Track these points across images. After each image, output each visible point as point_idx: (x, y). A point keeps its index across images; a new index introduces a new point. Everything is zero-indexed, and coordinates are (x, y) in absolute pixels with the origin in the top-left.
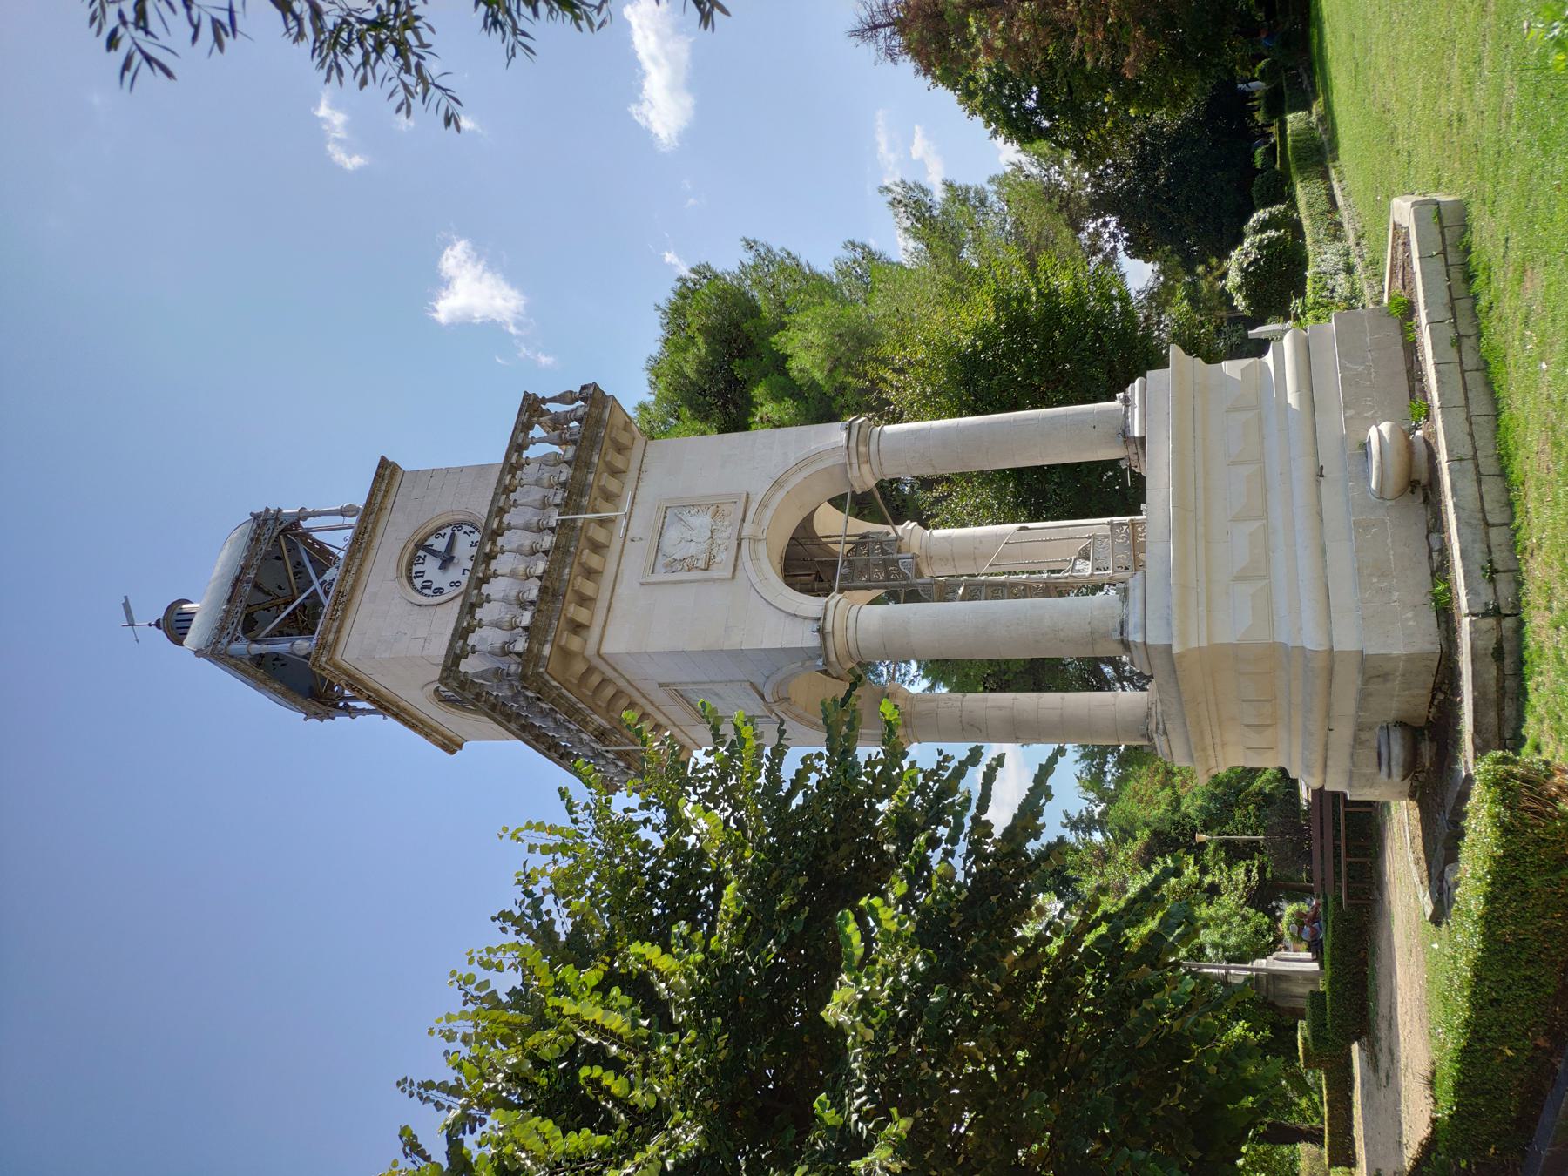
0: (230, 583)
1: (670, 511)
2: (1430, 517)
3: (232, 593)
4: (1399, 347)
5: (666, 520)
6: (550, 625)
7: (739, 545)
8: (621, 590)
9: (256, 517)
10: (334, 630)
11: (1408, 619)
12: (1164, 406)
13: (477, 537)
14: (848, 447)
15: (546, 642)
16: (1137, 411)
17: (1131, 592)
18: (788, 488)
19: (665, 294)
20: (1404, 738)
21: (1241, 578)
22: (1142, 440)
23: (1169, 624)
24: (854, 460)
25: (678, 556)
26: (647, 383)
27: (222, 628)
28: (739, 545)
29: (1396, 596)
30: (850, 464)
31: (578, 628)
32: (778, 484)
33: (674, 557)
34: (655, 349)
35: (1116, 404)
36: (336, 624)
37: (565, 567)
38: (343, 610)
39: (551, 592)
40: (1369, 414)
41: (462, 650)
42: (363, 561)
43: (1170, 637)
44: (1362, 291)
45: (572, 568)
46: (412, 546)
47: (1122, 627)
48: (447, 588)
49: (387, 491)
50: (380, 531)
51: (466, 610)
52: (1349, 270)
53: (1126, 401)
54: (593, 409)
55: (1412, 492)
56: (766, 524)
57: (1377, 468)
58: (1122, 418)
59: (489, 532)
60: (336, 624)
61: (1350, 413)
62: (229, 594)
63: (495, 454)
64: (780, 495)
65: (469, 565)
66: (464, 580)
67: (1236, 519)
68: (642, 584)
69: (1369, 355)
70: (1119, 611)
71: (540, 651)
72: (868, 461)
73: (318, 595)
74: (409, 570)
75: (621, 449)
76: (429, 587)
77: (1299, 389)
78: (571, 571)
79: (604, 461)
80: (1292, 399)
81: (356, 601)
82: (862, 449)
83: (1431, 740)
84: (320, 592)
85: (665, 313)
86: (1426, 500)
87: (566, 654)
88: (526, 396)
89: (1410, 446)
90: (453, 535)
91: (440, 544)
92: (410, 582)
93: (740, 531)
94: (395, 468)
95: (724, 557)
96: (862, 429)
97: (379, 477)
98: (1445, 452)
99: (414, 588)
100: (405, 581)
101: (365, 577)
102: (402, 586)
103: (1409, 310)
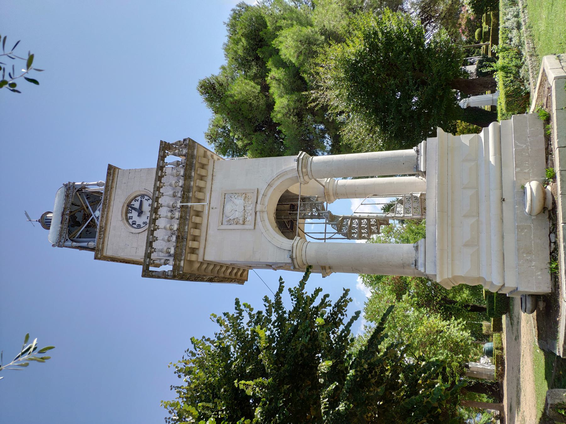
0: (60, 215)
1: (226, 196)
2: (551, 225)
3: (62, 219)
4: (543, 136)
5: (226, 200)
6: (182, 252)
7: (256, 213)
8: (210, 232)
9: (66, 185)
10: (101, 243)
11: (538, 275)
12: (434, 157)
13: (150, 202)
14: (298, 170)
15: (181, 260)
16: (422, 157)
17: (419, 247)
18: (274, 187)
19: (227, 16)
20: (532, 301)
21: (466, 245)
22: (425, 172)
23: (435, 265)
24: (301, 175)
25: (231, 218)
26: (224, 56)
27: (60, 235)
28: (256, 213)
29: (534, 264)
30: (299, 176)
31: (193, 251)
32: (270, 185)
33: (230, 218)
34: (226, 40)
35: (411, 152)
36: (101, 240)
37: (185, 225)
38: (103, 234)
39: (181, 238)
40: (527, 171)
41: (149, 262)
42: (108, 212)
43: (436, 272)
44: (524, 42)
45: (188, 226)
46: (126, 205)
47: (416, 262)
48: (142, 225)
49: (113, 180)
50: (113, 198)
51: (148, 245)
52: (519, 27)
53: (418, 151)
54: (190, 150)
55: (544, 212)
56: (266, 203)
57: (529, 206)
58: (416, 161)
59: (153, 209)
60: (101, 240)
61: (518, 169)
62: (61, 220)
63: (154, 165)
64: (271, 190)
65: (149, 214)
66: (148, 221)
67: (465, 216)
68: (218, 229)
69: (528, 140)
70: (414, 255)
71: (179, 264)
72: (307, 174)
73: (94, 220)
74: (126, 215)
75: (203, 166)
76: (135, 224)
77: (495, 154)
78: (188, 227)
79: (197, 174)
80: (492, 159)
81: (108, 230)
82: (304, 170)
83: (544, 301)
84: (95, 218)
85: (228, 25)
86: (550, 218)
87: (191, 262)
88: (161, 142)
89: (545, 193)
90: (141, 201)
91: (136, 205)
92: (128, 221)
93: (255, 208)
94: (115, 168)
95: (250, 218)
96: (304, 161)
97: (109, 174)
98: (562, 218)
99: (129, 224)
100: (125, 221)
101: (110, 219)
102: (124, 224)
103: (548, 120)
